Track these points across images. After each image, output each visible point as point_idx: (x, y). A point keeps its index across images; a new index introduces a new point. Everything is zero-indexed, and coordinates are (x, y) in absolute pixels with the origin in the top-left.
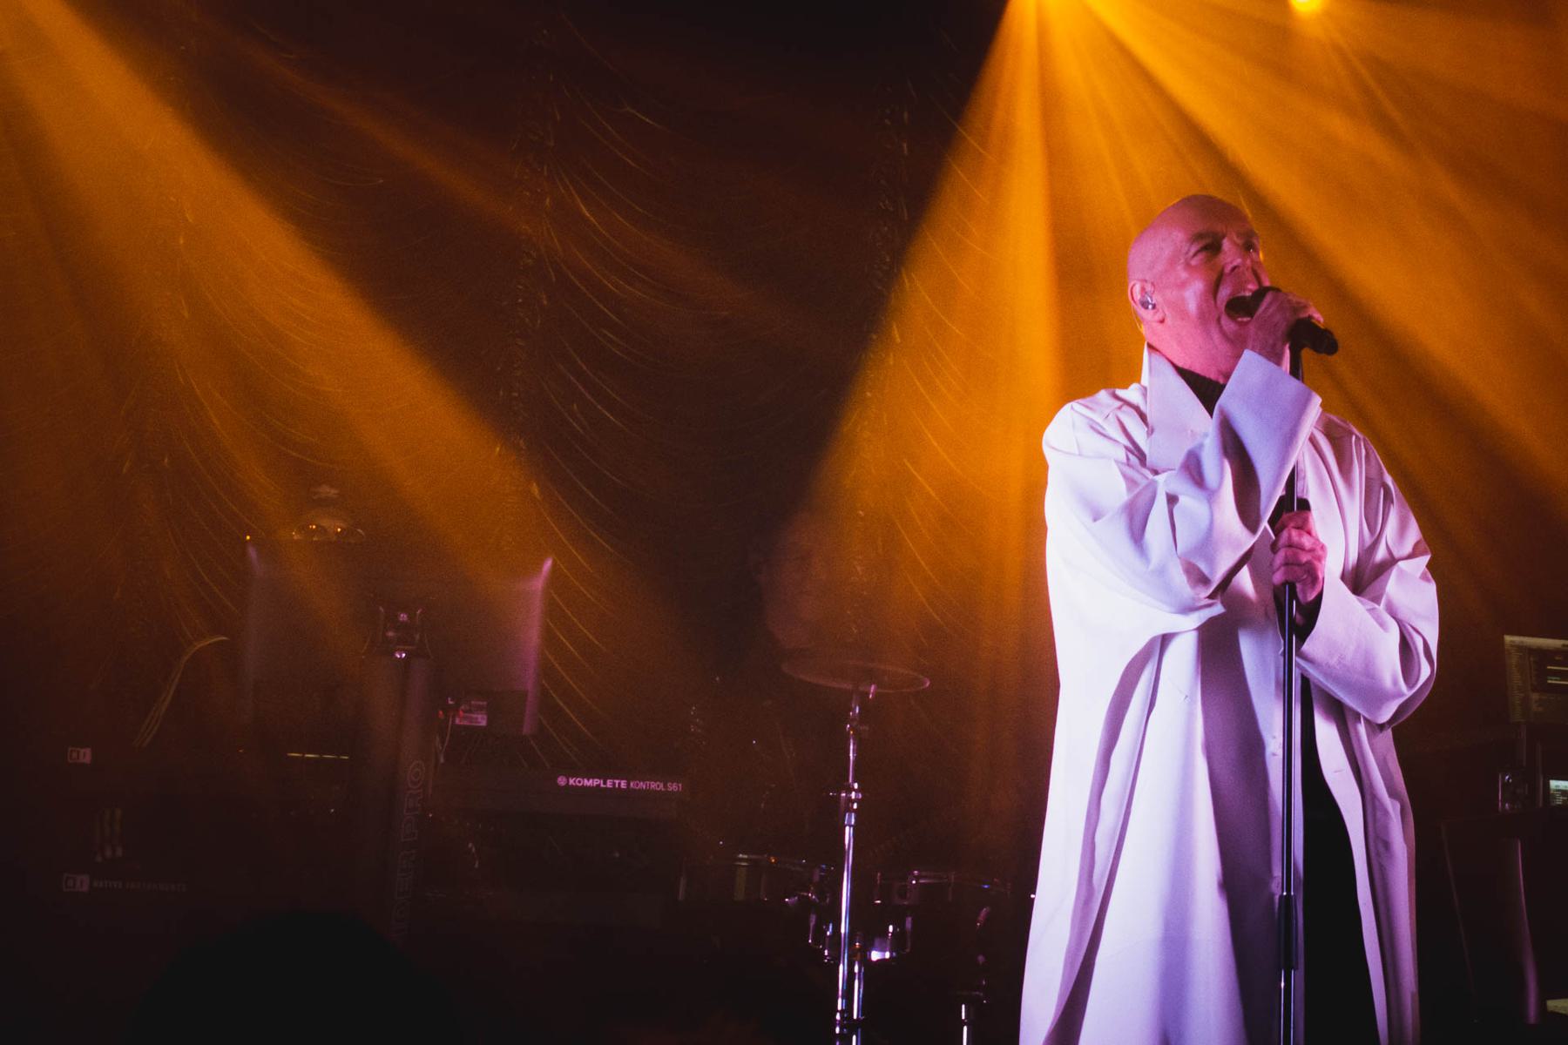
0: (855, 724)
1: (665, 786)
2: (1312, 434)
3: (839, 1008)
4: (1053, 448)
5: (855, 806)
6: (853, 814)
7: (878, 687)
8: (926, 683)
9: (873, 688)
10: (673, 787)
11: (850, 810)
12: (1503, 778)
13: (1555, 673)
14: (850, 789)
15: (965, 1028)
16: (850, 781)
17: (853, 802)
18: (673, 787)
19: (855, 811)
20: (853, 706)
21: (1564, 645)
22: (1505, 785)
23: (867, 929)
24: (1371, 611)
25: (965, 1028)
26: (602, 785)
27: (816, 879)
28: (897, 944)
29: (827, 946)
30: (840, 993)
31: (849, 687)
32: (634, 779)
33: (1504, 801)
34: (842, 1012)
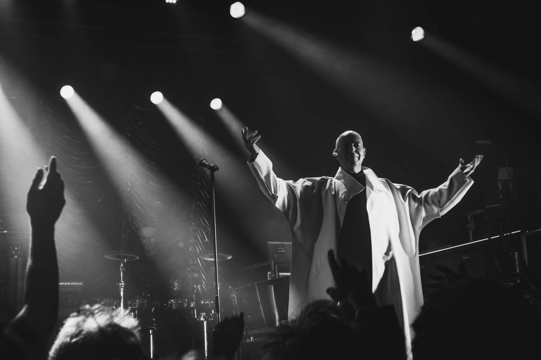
0: (122, 268)
1: (78, 284)
2: (336, 178)
7: (127, 259)
9: (126, 260)
10: (80, 284)
11: (122, 287)
13: (199, 249)
15: (512, 233)
18: (80, 284)
19: (123, 288)
21: (281, 243)
22: (269, 274)
24: (414, 204)
25: (512, 233)
26: (64, 284)
31: (120, 260)
32: (72, 282)
33: (269, 278)
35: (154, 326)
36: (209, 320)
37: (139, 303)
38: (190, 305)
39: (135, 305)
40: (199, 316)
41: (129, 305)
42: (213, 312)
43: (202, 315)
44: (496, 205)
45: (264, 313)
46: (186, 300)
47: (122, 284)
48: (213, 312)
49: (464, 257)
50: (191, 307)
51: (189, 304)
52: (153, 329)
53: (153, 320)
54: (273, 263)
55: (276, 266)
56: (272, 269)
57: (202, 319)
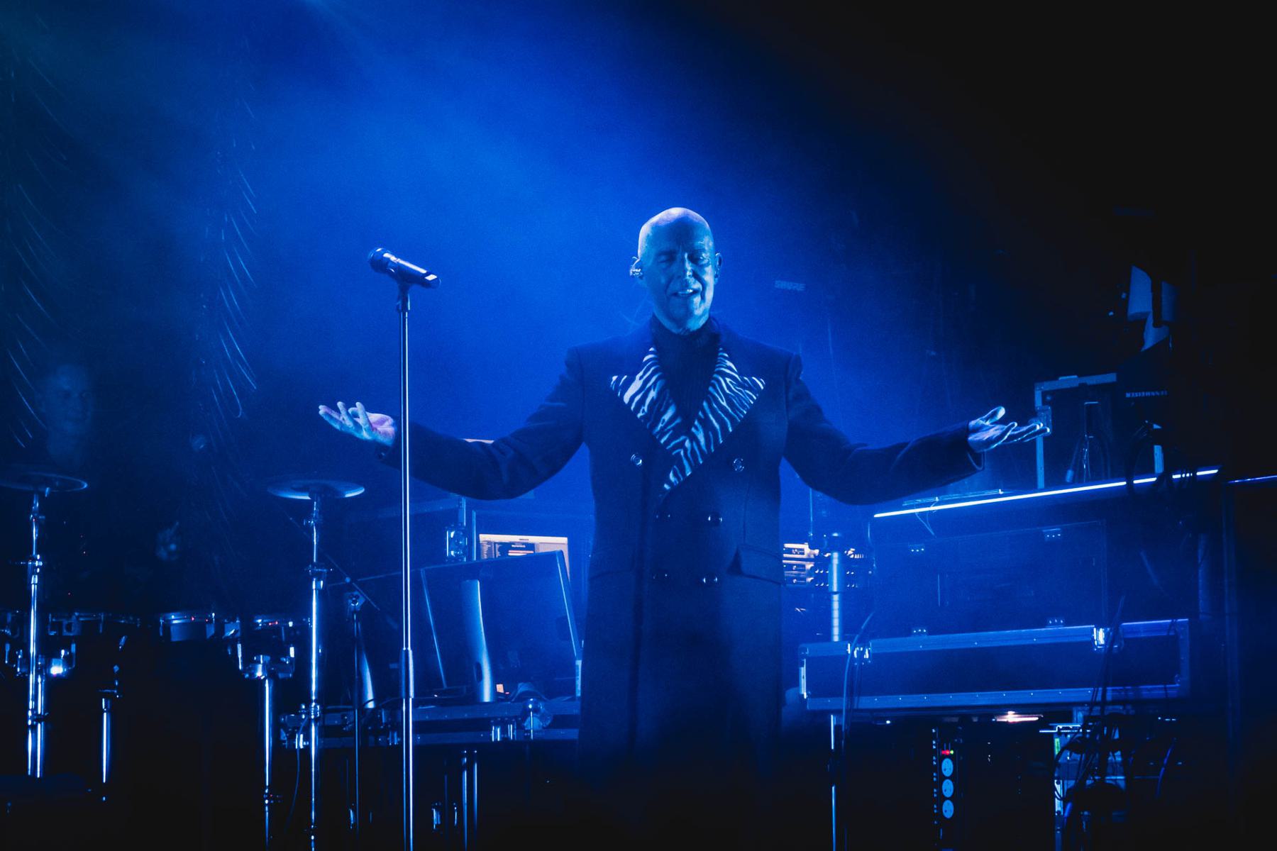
0: (36, 515)
3: (31, 707)
4: (755, 577)
5: (38, 570)
6: (36, 576)
8: (83, 486)
9: (47, 490)
12: (450, 534)
14: (34, 559)
16: (34, 553)
17: (37, 568)
20: (35, 502)
23: (48, 650)
27: (1110, 779)
28: (67, 661)
29: (19, 665)
30: (31, 698)
34: (32, 710)
35: (114, 687)
36: (281, 676)
37: (81, 619)
38: (223, 633)
39: (69, 628)
40: (250, 662)
41: (49, 627)
42: (292, 654)
43: (259, 662)
44: (1153, 394)
45: (442, 662)
46: (213, 614)
47: (37, 564)
48: (292, 654)
49: (1048, 533)
50: (228, 637)
51: (220, 629)
52: (109, 697)
53: (113, 670)
54: (464, 506)
55: (474, 514)
56: (462, 523)
57: (259, 673)
